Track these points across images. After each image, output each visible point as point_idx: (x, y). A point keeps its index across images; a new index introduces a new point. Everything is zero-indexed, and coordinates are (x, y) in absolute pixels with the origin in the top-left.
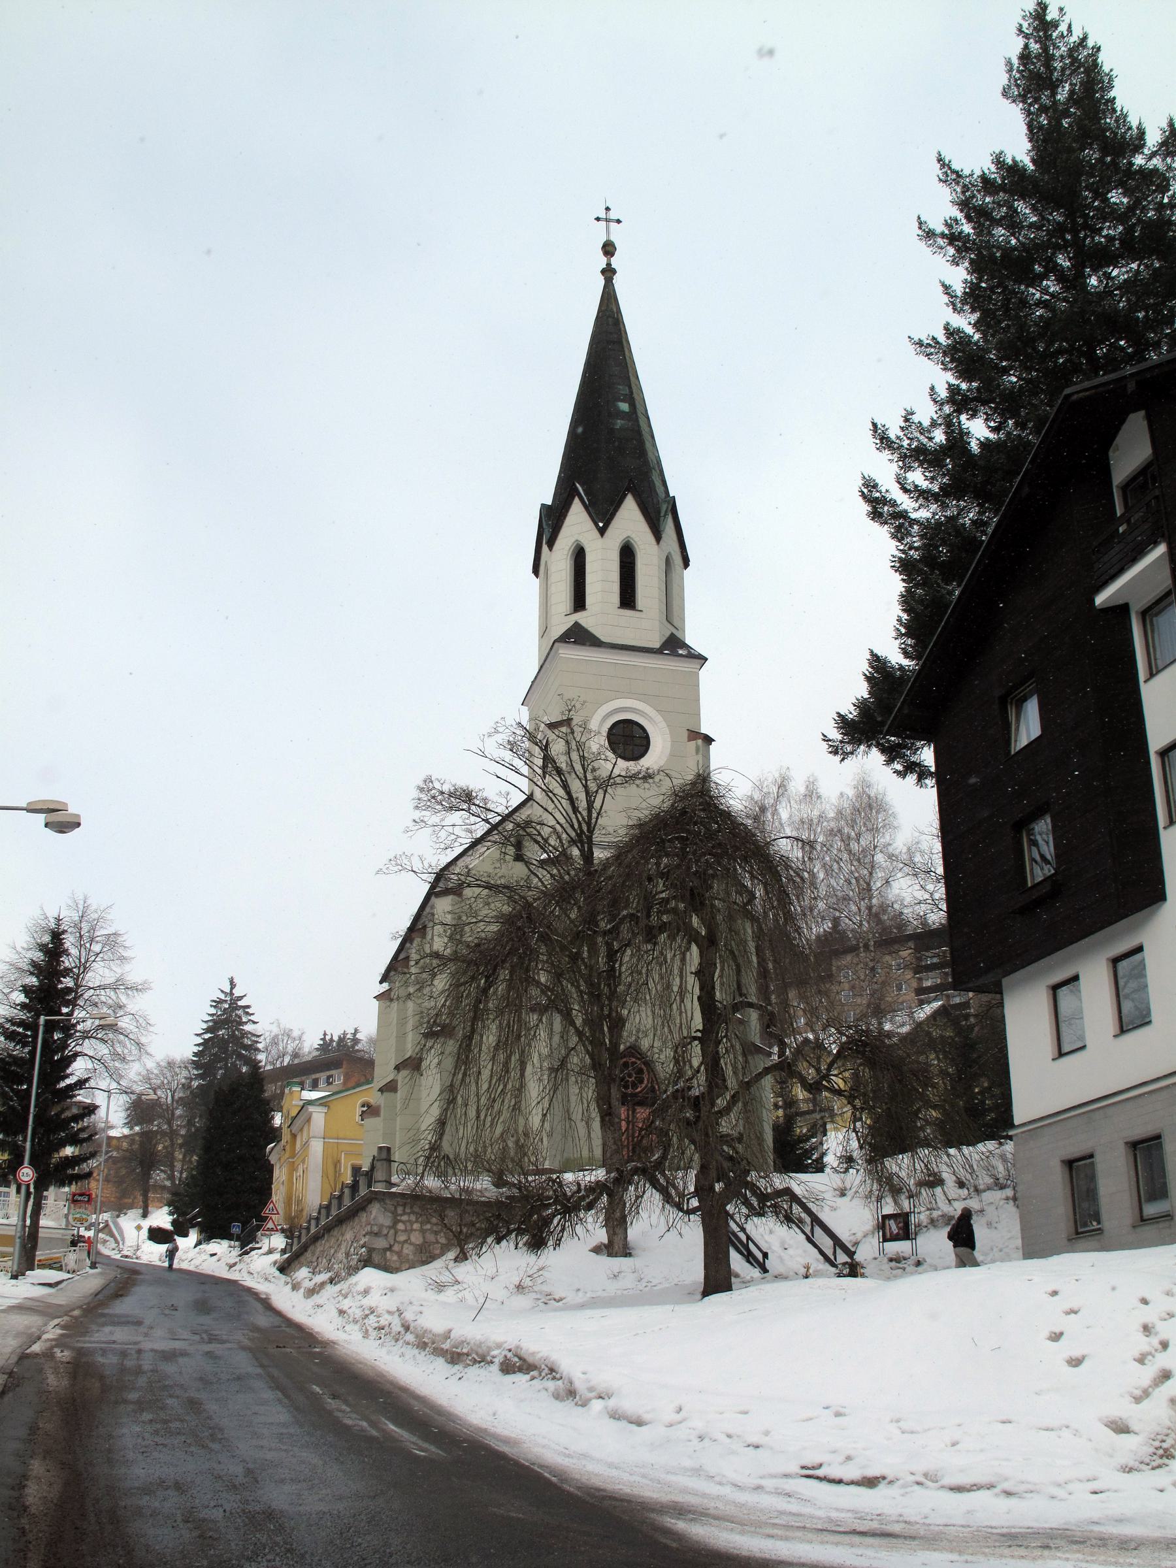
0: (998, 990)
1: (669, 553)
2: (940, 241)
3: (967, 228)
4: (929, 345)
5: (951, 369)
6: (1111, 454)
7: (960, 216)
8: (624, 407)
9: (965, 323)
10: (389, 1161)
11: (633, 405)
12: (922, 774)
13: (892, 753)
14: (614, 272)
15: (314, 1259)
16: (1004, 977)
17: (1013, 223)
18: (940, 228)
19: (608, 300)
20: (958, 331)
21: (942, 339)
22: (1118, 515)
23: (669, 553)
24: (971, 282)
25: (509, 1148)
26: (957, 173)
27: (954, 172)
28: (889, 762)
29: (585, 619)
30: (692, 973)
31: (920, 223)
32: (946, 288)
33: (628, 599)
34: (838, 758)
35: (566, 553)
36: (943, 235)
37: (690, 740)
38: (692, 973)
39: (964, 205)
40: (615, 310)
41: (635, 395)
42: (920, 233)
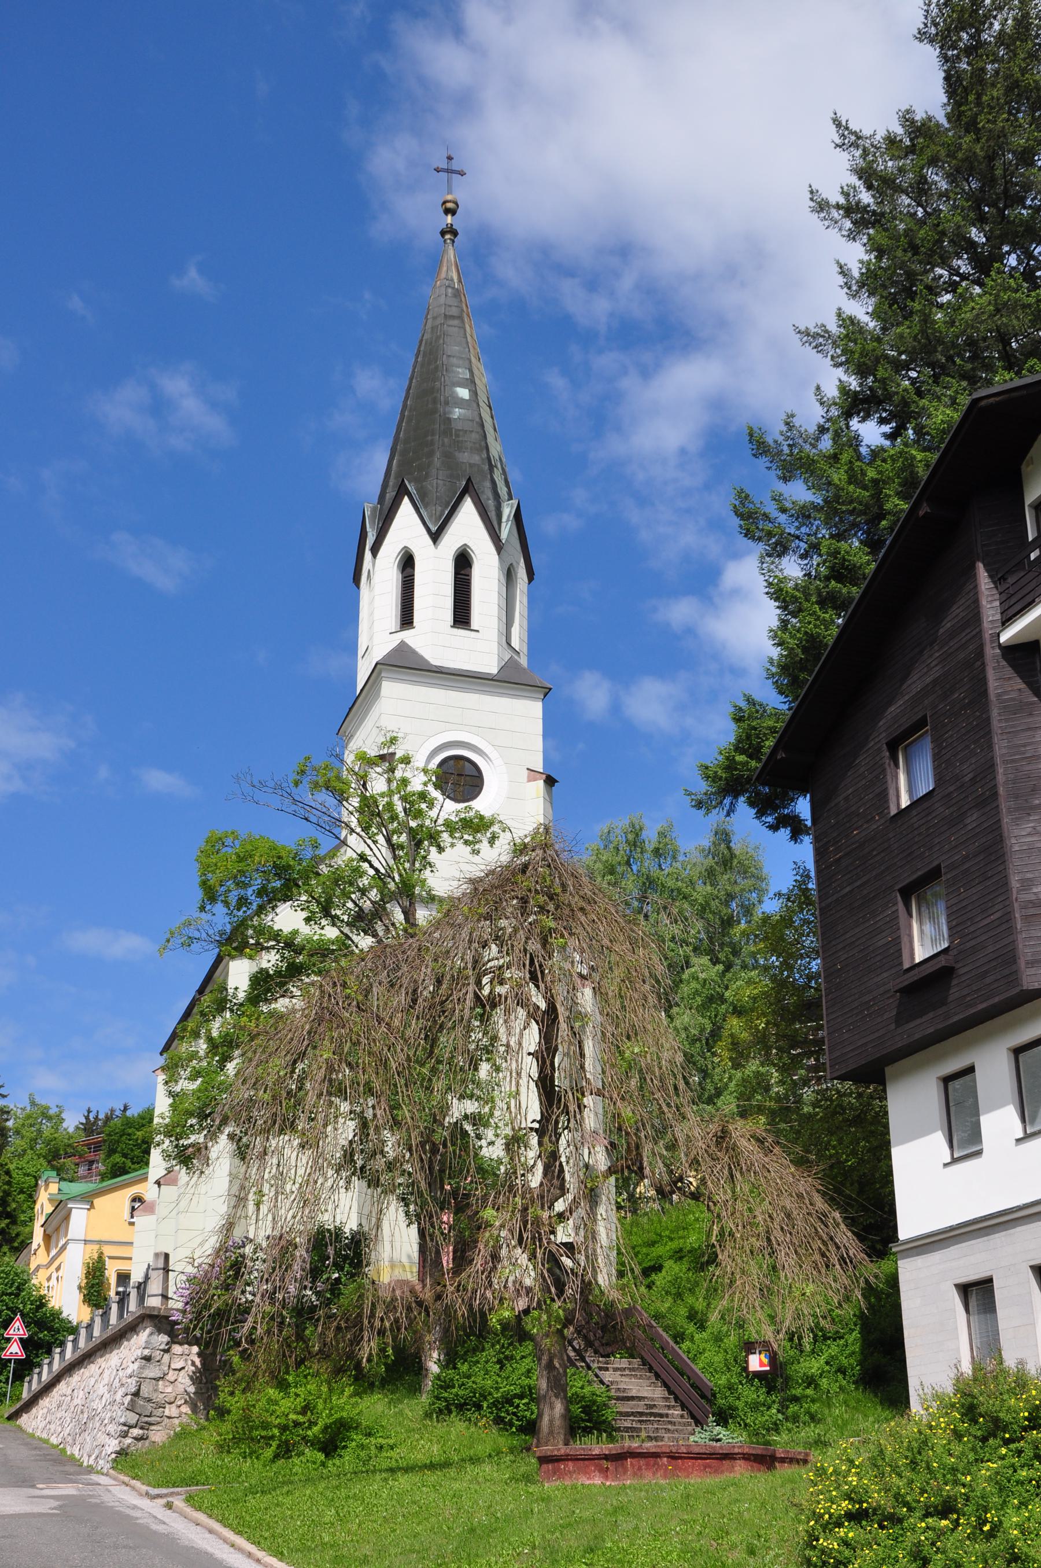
0: (881, 1081)
2: (835, 214)
3: (866, 197)
4: (817, 335)
5: (841, 364)
6: (1023, 467)
7: (859, 183)
9: (861, 310)
10: (166, 1270)
12: (797, 830)
13: (762, 806)
15: (69, 1392)
16: (888, 1065)
17: (921, 190)
18: (836, 197)
20: (852, 320)
21: (833, 327)
22: (1030, 539)
24: (869, 262)
25: (576, 1015)
26: (855, 133)
27: (852, 133)
28: (760, 814)
29: (413, 638)
30: (529, 1054)
31: (812, 192)
32: (843, 271)
33: (462, 616)
34: (703, 811)
36: (838, 207)
38: (529, 1054)
39: (867, 174)
42: (812, 204)
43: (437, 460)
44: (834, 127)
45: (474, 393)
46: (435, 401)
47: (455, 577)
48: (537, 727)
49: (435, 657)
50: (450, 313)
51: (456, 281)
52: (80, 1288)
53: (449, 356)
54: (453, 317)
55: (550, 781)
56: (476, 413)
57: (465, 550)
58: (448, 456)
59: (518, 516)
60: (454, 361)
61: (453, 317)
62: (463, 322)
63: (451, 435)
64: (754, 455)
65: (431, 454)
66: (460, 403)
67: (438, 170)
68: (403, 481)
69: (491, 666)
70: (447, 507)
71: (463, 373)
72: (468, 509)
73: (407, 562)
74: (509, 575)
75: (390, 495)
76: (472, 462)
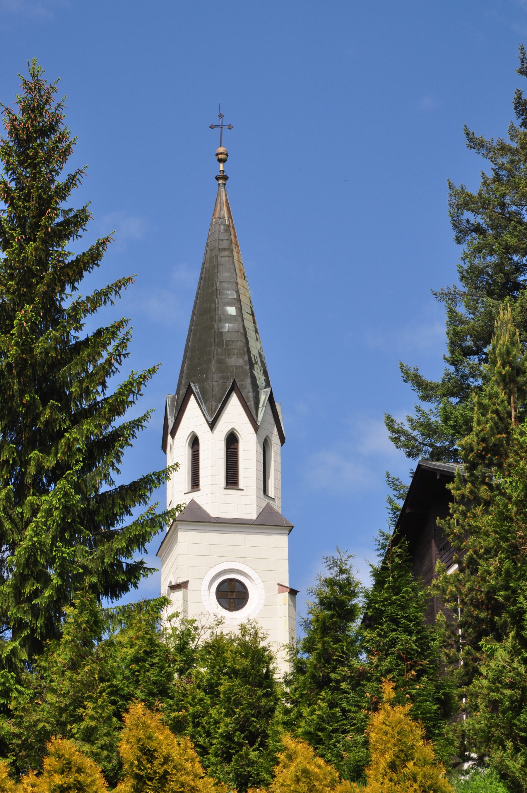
23: (267, 436)
43: (213, 366)
45: (240, 309)
46: (212, 319)
47: (227, 452)
48: (285, 554)
50: (223, 247)
51: (226, 218)
52: (124, 424)
53: (222, 282)
54: (224, 249)
55: (293, 593)
56: (241, 325)
57: (233, 431)
58: (220, 362)
59: (271, 400)
60: (225, 285)
61: (224, 249)
62: (232, 252)
63: (223, 346)
64: (405, 381)
65: (209, 361)
66: (230, 319)
67: (212, 127)
68: (190, 384)
69: (252, 515)
70: (219, 403)
71: (231, 294)
72: (234, 401)
73: (195, 442)
74: (265, 446)
75: (183, 391)
76: (238, 364)
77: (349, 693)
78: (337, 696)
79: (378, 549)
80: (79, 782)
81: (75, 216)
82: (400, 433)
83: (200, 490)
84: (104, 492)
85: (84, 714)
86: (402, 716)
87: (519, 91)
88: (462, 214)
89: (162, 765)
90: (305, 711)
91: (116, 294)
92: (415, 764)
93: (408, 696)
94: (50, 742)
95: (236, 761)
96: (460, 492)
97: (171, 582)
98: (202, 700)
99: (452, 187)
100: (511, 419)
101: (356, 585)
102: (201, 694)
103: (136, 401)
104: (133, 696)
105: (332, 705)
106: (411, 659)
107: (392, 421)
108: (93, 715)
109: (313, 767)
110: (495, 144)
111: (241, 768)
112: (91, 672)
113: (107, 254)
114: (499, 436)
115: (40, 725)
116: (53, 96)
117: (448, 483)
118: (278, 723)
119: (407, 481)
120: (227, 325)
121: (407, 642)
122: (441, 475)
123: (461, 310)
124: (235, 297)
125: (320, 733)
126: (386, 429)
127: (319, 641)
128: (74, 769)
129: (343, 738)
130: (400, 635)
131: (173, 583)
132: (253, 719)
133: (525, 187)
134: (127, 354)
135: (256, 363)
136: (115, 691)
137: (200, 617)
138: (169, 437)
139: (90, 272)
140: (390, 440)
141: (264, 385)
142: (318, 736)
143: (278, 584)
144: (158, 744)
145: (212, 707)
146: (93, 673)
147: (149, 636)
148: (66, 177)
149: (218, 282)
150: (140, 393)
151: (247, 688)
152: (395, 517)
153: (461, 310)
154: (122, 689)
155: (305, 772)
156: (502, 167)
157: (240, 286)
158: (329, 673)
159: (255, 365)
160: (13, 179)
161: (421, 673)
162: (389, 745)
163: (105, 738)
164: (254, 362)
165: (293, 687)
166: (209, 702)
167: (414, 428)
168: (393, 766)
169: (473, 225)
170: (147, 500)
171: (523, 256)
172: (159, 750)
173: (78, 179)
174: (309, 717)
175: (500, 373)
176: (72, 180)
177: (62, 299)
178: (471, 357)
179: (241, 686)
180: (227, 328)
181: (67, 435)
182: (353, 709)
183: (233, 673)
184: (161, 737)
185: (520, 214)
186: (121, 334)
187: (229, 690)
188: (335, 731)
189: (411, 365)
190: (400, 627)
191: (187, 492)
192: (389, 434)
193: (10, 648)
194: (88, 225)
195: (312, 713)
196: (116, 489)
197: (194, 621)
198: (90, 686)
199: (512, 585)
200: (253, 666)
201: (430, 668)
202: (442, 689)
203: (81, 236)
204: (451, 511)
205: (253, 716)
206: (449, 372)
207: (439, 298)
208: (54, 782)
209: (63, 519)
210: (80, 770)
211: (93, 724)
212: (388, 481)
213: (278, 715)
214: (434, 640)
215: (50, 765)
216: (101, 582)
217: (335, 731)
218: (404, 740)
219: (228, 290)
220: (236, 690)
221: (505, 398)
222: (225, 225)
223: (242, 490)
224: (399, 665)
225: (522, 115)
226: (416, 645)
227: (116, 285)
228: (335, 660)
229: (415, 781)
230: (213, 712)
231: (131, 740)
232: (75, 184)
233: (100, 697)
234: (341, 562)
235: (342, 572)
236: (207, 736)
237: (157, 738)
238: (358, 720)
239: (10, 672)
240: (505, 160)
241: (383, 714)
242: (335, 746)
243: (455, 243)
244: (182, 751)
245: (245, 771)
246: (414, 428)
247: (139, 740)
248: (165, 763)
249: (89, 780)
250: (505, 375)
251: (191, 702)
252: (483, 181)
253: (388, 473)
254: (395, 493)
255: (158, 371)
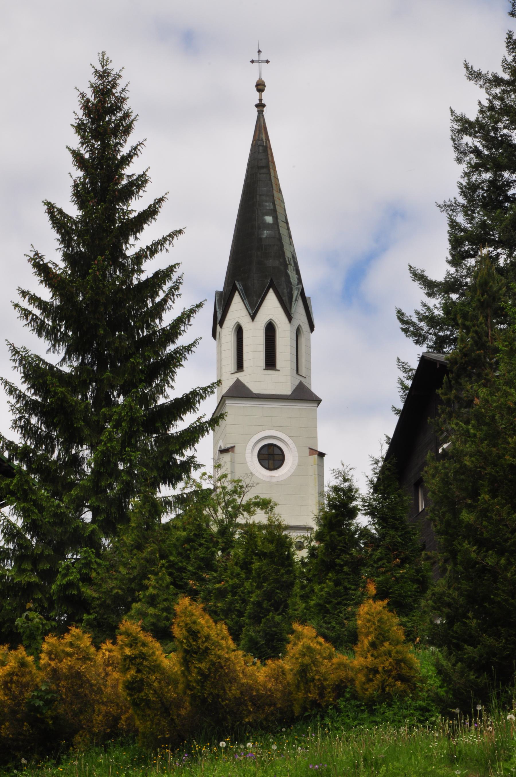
1: (300, 325)
8: (269, 219)
11: (276, 218)
14: (264, 106)
19: (259, 131)
23: (300, 325)
35: (231, 330)
37: (311, 454)
40: (264, 138)
41: (278, 209)
44: (465, 69)
49: (255, 389)
51: (264, 140)
53: (260, 195)
64: (413, 280)
66: (268, 226)
68: (235, 282)
70: (259, 298)
72: (271, 297)
73: (239, 331)
77: (350, 575)
78: (340, 576)
79: (372, 464)
80: (143, 653)
81: (137, 179)
82: (409, 324)
83: (243, 371)
84: (161, 403)
85: (129, 766)
86: (381, 608)
87: (510, 32)
88: (462, 138)
89: (203, 642)
90: (317, 588)
91: (170, 244)
92: (390, 644)
93: (393, 578)
94: (122, 624)
95: (265, 623)
96: (446, 397)
97: (220, 447)
98: (238, 574)
99: (454, 114)
100: (488, 337)
101: (357, 490)
102: (237, 570)
103: (186, 330)
104: (185, 569)
105: (337, 583)
106: (397, 550)
107: (403, 314)
108: (155, 585)
109: (315, 645)
110: (490, 76)
111: (268, 628)
112: (152, 553)
113: (163, 210)
114: (478, 352)
115: (115, 591)
116: (118, 81)
117: (438, 389)
118: (296, 595)
119: (415, 364)
120: (265, 232)
121: (393, 537)
122: (440, 365)
123: (460, 219)
124: (272, 208)
125: (327, 605)
126: (398, 321)
127: (327, 535)
128: (139, 644)
129: (345, 609)
130: (388, 531)
131: (223, 448)
132: (277, 591)
133: (515, 116)
134: (180, 295)
135: (290, 264)
136: (172, 565)
137: (245, 478)
138: (218, 326)
139: (149, 225)
140: (401, 330)
141: (296, 282)
142: (326, 607)
143: (309, 448)
144: (201, 627)
145: (246, 580)
146: (155, 553)
147: (197, 523)
148: (130, 149)
149: (258, 196)
150: (190, 323)
151: (272, 567)
152: (405, 395)
153: (460, 219)
154: (177, 563)
155: (309, 648)
156: (495, 97)
157: (276, 199)
158: (335, 559)
159: (289, 266)
160: (87, 151)
161: (404, 561)
162: (371, 630)
163: (165, 603)
164: (288, 263)
165: (308, 567)
166: (244, 576)
167: (420, 320)
168: (373, 645)
169: (471, 147)
170: (196, 410)
171: (513, 173)
172: (202, 632)
173: (139, 150)
174: (320, 593)
175: (479, 300)
176: (134, 151)
177: (127, 248)
178: (469, 259)
179: (268, 565)
180: (266, 234)
181: (132, 360)
182: (353, 587)
183: (262, 555)
184: (203, 622)
185: (511, 136)
186: (175, 277)
187: (259, 568)
188: (339, 603)
189: (419, 267)
190: (389, 525)
191: (233, 372)
192: (400, 325)
193: (90, 529)
194: (148, 186)
195: (321, 590)
196: (171, 401)
197: (239, 481)
198: (151, 562)
199: (450, 531)
200: (277, 550)
201: (412, 556)
202: (421, 572)
203: (141, 197)
204: (440, 411)
205: (277, 589)
206: (450, 272)
207: (442, 209)
208: (125, 653)
209: (130, 428)
210: (144, 645)
211: (155, 592)
212: (399, 365)
213: (297, 589)
214: (415, 534)
215: (121, 641)
216: (160, 475)
217: (339, 603)
218: (383, 626)
219: (266, 202)
220: (264, 568)
221: (483, 321)
222: (263, 146)
223: (279, 370)
224: (387, 555)
225: (513, 52)
226: (401, 539)
227: (170, 236)
228: (339, 549)
229: (391, 656)
230: (247, 584)
231: (180, 624)
232: (137, 155)
233: (160, 572)
234: (345, 473)
235: (345, 480)
236: (242, 603)
237: (200, 623)
238: (356, 597)
239: (90, 549)
240: (497, 91)
241: (367, 607)
242: (339, 616)
243: (456, 163)
244: (219, 632)
245: (272, 631)
246: (420, 320)
247: (187, 624)
248: (206, 641)
249: (151, 651)
250: (483, 302)
251: (230, 575)
252: (479, 108)
253: (398, 359)
254: (405, 375)
255: (204, 306)
